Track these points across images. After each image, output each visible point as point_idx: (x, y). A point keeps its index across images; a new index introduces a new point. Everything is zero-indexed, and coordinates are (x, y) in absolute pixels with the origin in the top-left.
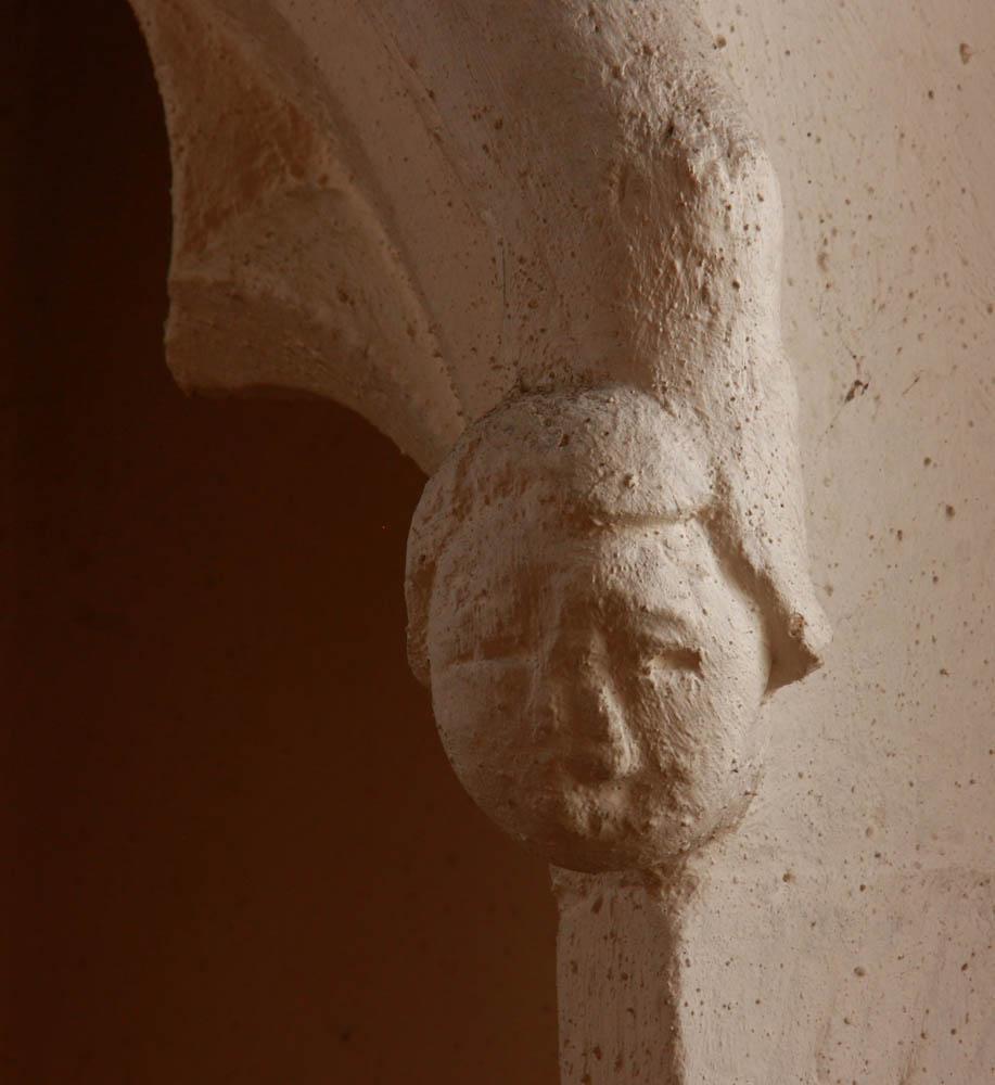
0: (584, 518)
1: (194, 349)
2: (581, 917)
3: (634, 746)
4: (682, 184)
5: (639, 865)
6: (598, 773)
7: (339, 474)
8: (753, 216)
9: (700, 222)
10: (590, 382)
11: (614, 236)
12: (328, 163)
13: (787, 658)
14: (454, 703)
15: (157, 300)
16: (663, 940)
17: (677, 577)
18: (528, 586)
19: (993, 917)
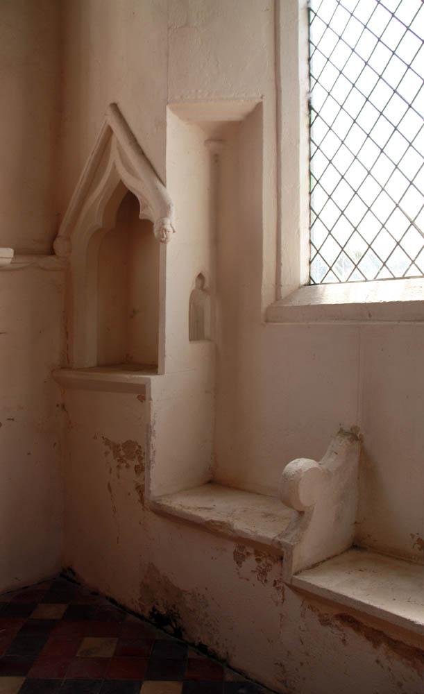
0: (163, 224)
1: (141, 217)
2: (162, 245)
3: (89, 167)
4: (170, 207)
5: (165, 242)
6: (163, 237)
7: (148, 224)
8: (173, 209)
9: (154, 436)
10: (164, 217)
11: (165, 209)
12: (149, 207)
13: (174, 232)
14: (156, 234)
15: (139, 214)
16: (166, 247)
17: (168, 227)
18: (160, 228)
19: (408, 299)
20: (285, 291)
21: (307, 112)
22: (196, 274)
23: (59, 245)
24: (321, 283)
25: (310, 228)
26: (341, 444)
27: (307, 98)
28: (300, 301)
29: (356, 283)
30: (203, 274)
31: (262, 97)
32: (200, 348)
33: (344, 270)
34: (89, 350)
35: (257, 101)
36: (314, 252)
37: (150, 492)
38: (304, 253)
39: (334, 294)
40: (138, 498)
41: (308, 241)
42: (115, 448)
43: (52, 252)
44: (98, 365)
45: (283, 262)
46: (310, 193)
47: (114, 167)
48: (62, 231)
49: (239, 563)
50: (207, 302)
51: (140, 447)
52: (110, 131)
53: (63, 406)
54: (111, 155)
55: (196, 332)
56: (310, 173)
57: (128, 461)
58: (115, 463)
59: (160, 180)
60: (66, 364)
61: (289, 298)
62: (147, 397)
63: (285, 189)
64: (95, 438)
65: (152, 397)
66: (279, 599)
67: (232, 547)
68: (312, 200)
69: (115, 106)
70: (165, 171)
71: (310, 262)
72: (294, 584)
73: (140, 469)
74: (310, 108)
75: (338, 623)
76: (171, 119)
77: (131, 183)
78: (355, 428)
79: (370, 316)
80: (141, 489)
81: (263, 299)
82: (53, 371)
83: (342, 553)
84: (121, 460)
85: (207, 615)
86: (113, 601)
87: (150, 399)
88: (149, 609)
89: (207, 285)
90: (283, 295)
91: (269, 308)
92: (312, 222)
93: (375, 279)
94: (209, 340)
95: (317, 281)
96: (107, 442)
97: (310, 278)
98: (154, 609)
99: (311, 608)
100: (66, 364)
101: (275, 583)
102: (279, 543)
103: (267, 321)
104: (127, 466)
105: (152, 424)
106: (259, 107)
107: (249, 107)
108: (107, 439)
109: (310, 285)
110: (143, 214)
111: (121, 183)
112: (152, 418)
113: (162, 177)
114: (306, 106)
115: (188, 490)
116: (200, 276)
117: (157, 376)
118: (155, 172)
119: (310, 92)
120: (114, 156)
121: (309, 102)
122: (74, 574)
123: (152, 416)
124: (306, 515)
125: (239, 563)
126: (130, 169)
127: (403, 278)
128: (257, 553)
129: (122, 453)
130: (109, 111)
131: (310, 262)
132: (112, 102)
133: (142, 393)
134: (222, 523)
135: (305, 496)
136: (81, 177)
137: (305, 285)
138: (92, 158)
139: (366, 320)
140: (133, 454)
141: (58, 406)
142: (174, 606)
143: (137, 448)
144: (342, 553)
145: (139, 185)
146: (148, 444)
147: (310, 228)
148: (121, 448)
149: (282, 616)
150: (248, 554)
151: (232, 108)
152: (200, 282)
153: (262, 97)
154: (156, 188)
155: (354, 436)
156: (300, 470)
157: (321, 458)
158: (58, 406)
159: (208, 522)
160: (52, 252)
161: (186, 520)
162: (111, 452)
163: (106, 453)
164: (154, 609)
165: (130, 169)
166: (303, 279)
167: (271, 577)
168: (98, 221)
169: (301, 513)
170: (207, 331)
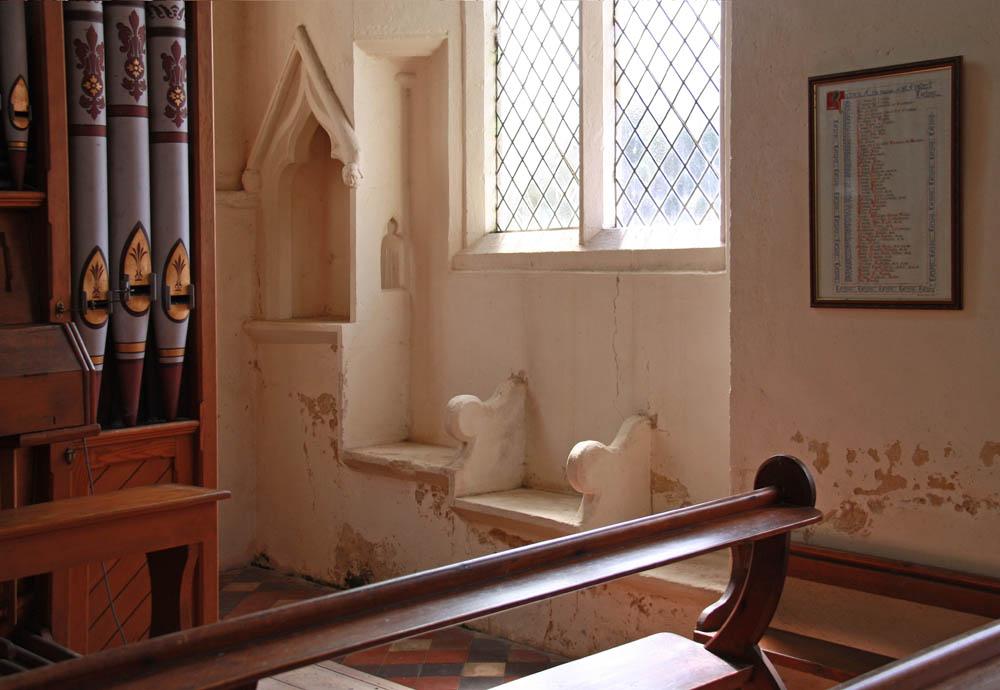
0: (351, 170)
2: (351, 190)
5: (354, 188)
8: (361, 155)
11: (353, 154)
14: (345, 179)
20: (470, 238)
21: (493, 50)
22: (386, 220)
23: (248, 179)
24: (506, 231)
25: (497, 173)
26: (507, 386)
27: (493, 34)
28: (481, 250)
29: (64, 339)
30: (396, 219)
31: (447, 34)
32: (393, 296)
33: (524, 218)
34: (283, 299)
35: (444, 37)
36: (500, 198)
37: (342, 442)
38: (490, 199)
39: (508, 245)
40: (333, 454)
41: (494, 187)
42: (311, 404)
43: (241, 187)
44: (293, 317)
45: (468, 209)
46: (497, 136)
47: (305, 97)
48: (251, 164)
49: (419, 502)
50: (400, 248)
51: (334, 399)
52: (298, 58)
53: (256, 364)
54: (302, 84)
55: (389, 280)
56: (497, 115)
57: (324, 417)
58: (310, 420)
59: (350, 123)
60: (258, 316)
61: (474, 245)
62: (339, 345)
63: (470, 132)
64: (290, 395)
65: (344, 344)
66: (450, 529)
67: (413, 487)
68: (499, 143)
69: (302, 28)
70: (353, 113)
71: (497, 209)
72: (457, 505)
73: (334, 423)
74: (497, 44)
75: (491, 538)
76: (358, 55)
77: (321, 118)
78: (522, 373)
79: (532, 265)
80: (334, 444)
81: (450, 247)
82: (245, 323)
83: (509, 490)
84: (316, 417)
85: (395, 565)
86: (309, 578)
87: (342, 347)
88: (344, 574)
89: (400, 231)
90: (469, 243)
91: (456, 256)
92: (618, 107)
93: (548, 229)
94: (404, 288)
95: (503, 229)
96: (303, 398)
97: (497, 225)
98: (349, 574)
99: (473, 530)
100: (258, 316)
101: (447, 514)
102: (445, 471)
103: (454, 269)
104: (323, 422)
105: (343, 372)
106: (445, 43)
107: (436, 44)
108: (302, 395)
109: (497, 232)
110: (335, 153)
111: (312, 116)
112: (344, 366)
113: (351, 119)
114: (492, 42)
115: (381, 445)
116: (393, 220)
117: (349, 324)
118: (344, 113)
119: (497, 26)
120: (304, 85)
121: (496, 38)
122: (268, 559)
123: (344, 364)
124: (469, 446)
125: (419, 502)
126: (320, 104)
127: (569, 228)
128: (433, 489)
129: (317, 408)
130: (298, 35)
131: (497, 209)
132: (299, 24)
133: (334, 342)
134: (404, 462)
135: (465, 427)
136: (271, 103)
137: (491, 233)
138: (282, 84)
139: (527, 269)
140: (327, 408)
141: (250, 363)
142: (367, 565)
143: (332, 401)
144: (509, 490)
145: (329, 121)
146: (340, 392)
147: (497, 173)
148: (316, 403)
149: (453, 545)
150: (427, 491)
151: (420, 45)
152: (393, 226)
153: (447, 34)
154: (345, 131)
155: (520, 379)
156: (461, 402)
157: (612, 441)
158: (250, 363)
159: (391, 463)
160: (241, 187)
161: (374, 465)
162: (307, 409)
163: (302, 411)
164: (349, 574)
165: (320, 104)
166: (489, 226)
167: (444, 509)
168: (290, 156)
169: (465, 444)
170: (402, 281)
